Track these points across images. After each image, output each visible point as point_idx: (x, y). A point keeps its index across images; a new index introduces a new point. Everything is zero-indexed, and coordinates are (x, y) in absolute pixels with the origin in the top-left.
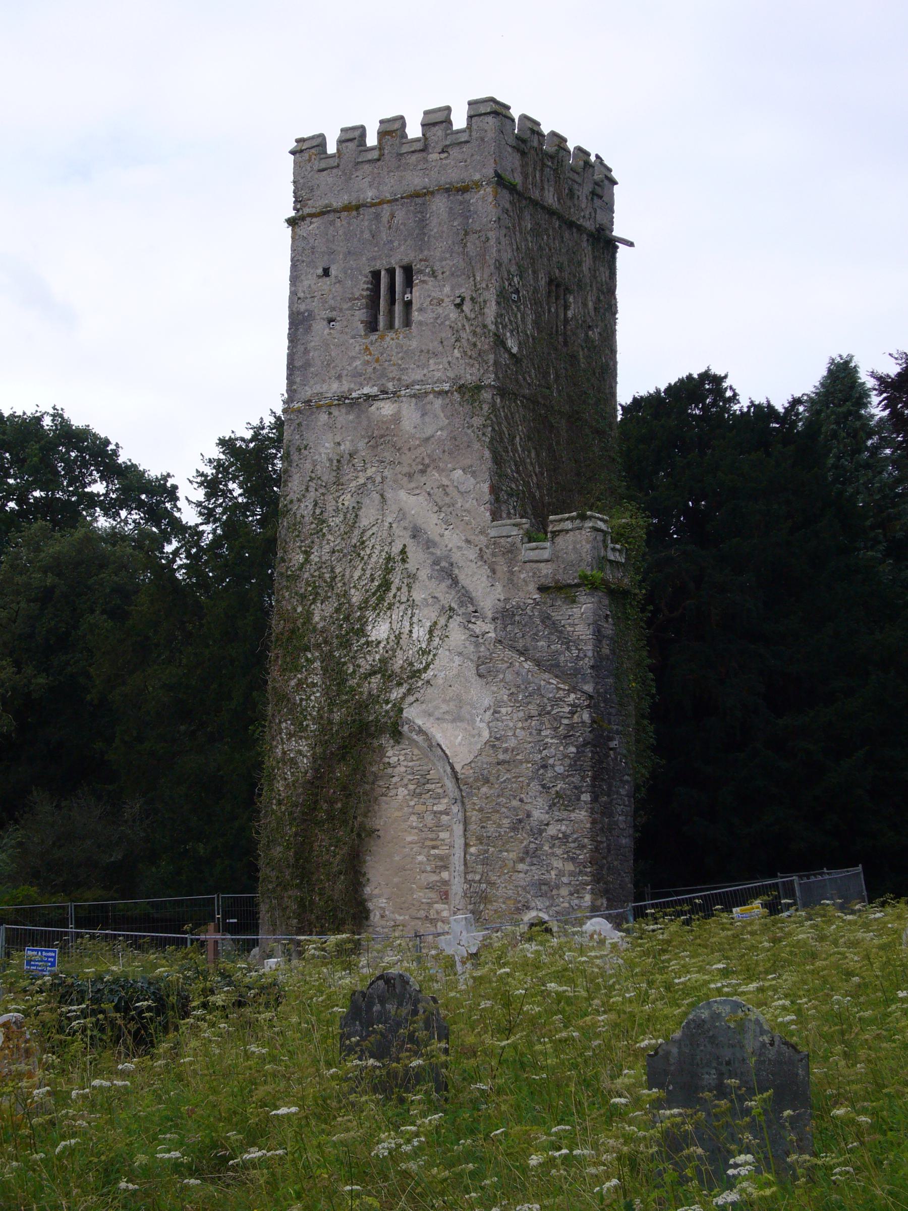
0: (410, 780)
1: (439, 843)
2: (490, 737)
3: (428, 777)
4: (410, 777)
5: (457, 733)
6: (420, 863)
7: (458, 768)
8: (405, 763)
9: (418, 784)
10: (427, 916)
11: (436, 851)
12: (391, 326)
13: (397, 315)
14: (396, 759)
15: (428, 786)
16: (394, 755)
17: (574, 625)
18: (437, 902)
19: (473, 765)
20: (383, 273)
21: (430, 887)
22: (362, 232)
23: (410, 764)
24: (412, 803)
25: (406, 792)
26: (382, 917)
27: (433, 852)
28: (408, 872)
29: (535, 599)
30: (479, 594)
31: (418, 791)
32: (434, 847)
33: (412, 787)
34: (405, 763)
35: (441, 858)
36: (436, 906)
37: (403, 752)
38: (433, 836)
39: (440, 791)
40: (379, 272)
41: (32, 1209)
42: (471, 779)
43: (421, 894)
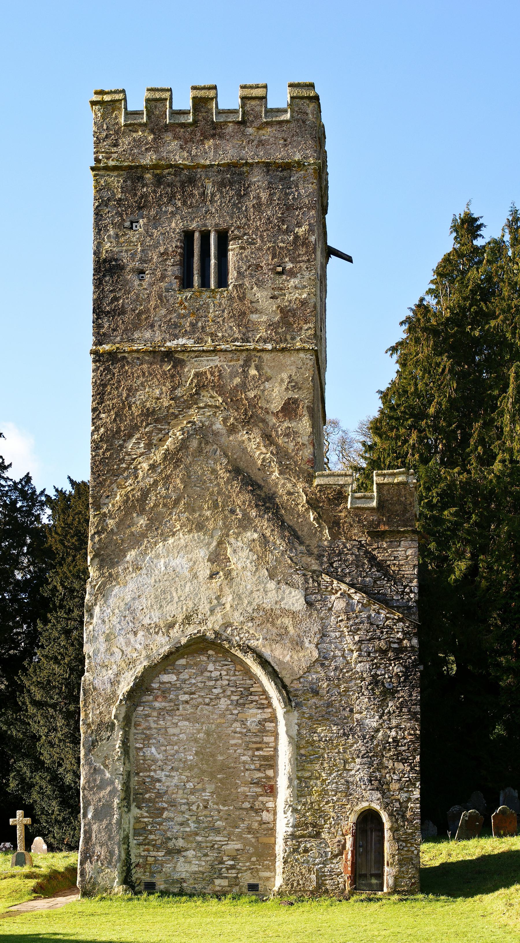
0: (232, 692)
1: (264, 746)
2: (319, 656)
3: (252, 689)
4: (232, 689)
5: (285, 652)
6: (244, 763)
7: (287, 681)
8: (228, 677)
9: (242, 695)
10: (251, 807)
11: (261, 753)
12: (205, 283)
13: (195, 272)
14: (218, 673)
15: (250, 698)
16: (216, 669)
17: (400, 566)
18: (261, 795)
19: (302, 680)
20: (197, 235)
21: (257, 783)
22: (238, 228)
23: (233, 678)
24: (235, 712)
25: (229, 702)
26: (206, 807)
27: (257, 753)
28: (232, 770)
29: (360, 542)
30: (304, 533)
31: (241, 701)
32: (258, 749)
33: (234, 698)
34: (228, 677)
35: (265, 758)
36: (260, 798)
37: (225, 667)
38: (258, 739)
39: (265, 702)
40: (192, 233)
41: (517, 492)
42: (300, 692)
43: (246, 789)
